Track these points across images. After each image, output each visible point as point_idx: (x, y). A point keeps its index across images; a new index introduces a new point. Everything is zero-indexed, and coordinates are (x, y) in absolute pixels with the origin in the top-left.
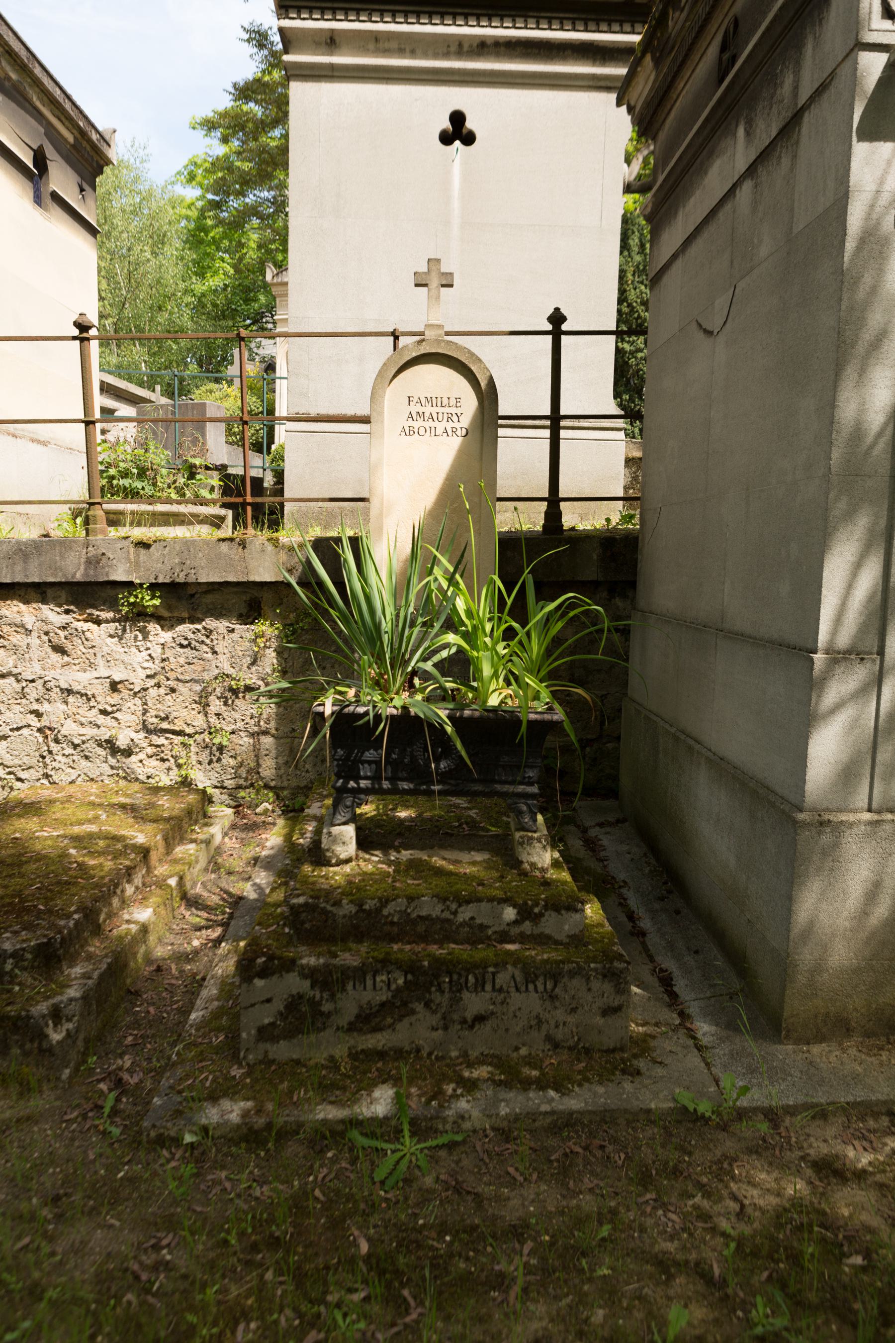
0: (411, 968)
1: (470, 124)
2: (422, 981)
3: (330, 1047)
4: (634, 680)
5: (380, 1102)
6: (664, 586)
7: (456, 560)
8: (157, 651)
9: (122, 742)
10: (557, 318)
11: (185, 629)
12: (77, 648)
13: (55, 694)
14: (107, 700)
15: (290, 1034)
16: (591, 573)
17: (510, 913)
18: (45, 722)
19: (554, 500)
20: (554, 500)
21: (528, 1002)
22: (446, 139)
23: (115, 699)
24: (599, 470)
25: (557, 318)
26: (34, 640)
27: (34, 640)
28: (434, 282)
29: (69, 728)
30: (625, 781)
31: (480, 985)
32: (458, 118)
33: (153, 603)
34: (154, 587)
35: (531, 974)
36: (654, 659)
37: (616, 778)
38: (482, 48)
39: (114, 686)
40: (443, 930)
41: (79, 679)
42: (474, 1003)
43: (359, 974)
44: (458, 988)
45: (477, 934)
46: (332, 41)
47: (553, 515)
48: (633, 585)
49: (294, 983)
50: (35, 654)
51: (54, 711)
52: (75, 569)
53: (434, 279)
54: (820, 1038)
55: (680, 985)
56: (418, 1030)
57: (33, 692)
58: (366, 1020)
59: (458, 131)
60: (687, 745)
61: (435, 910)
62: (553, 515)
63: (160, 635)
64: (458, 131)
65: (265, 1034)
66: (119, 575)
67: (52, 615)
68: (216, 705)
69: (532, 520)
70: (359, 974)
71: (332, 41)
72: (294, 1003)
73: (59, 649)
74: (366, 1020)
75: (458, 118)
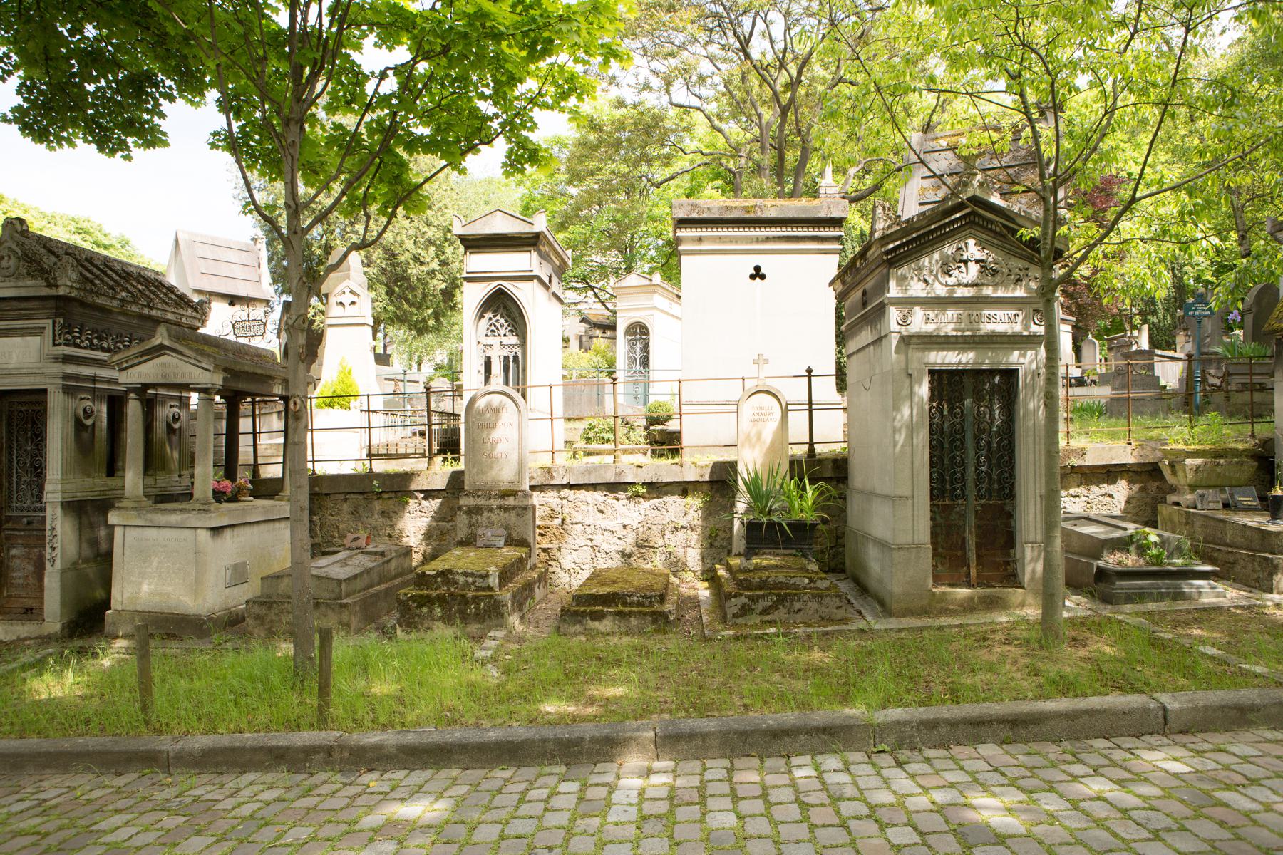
0: (778, 595)
1: (762, 271)
2: (781, 599)
3: (755, 619)
4: (849, 519)
5: (773, 630)
6: (858, 478)
7: (149, 324)
8: (643, 512)
9: (627, 552)
10: (809, 371)
11: (655, 501)
12: (608, 511)
13: (599, 531)
14: (621, 533)
15: (742, 616)
16: (829, 474)
17: (806, 581)
18: (594, 543)
19: (811, 444)
20: (811, 444)
21: (813, 605)
22: (752, 277)
23: (625, 532)
24: (831, 432)
25: (809, 371)
26: (590, 508)
27: (590, 508)
28: (761, 362)
29: (605, 546)
30: (847, 562)
31: (799, 600)
32: (757, 269)
33: (642, 490)
34: (643, 484)
35: (814, 597)
36: (855, 506)
37: (843, 564)
38: (767, 239)
39: (625, 527)
40: (788, 586)
41: (609, 524)
42: (797, 605)
43: (763, 596)
44: (792, 601)
45: (796, 587)
46: (700, 240)
47: (811, 449)
48: (846, 478)
49: (744, 600)
50: (591, 513)
51: (598, 539)
52: (610, 478)
53: (760, 360)
54: (904, 616)
55: (864, 612)
56: (780, 614)
57: (589, 530)
58: (765, 611)
59: (758, 274)
60: (867, 537)
61: (784, 580)
62: (811, 449)
63: (646, 505)
64: (758, 274)
65: (735, 616)
66: (629, 480)
67: (598, 496)
68: (668, 535)
69: (801, 451)
70: (763, 596)
71: (700, 240)
72: (743, 607)
73: (602, 512)
74: (765, 611)
75: (757, 269)
